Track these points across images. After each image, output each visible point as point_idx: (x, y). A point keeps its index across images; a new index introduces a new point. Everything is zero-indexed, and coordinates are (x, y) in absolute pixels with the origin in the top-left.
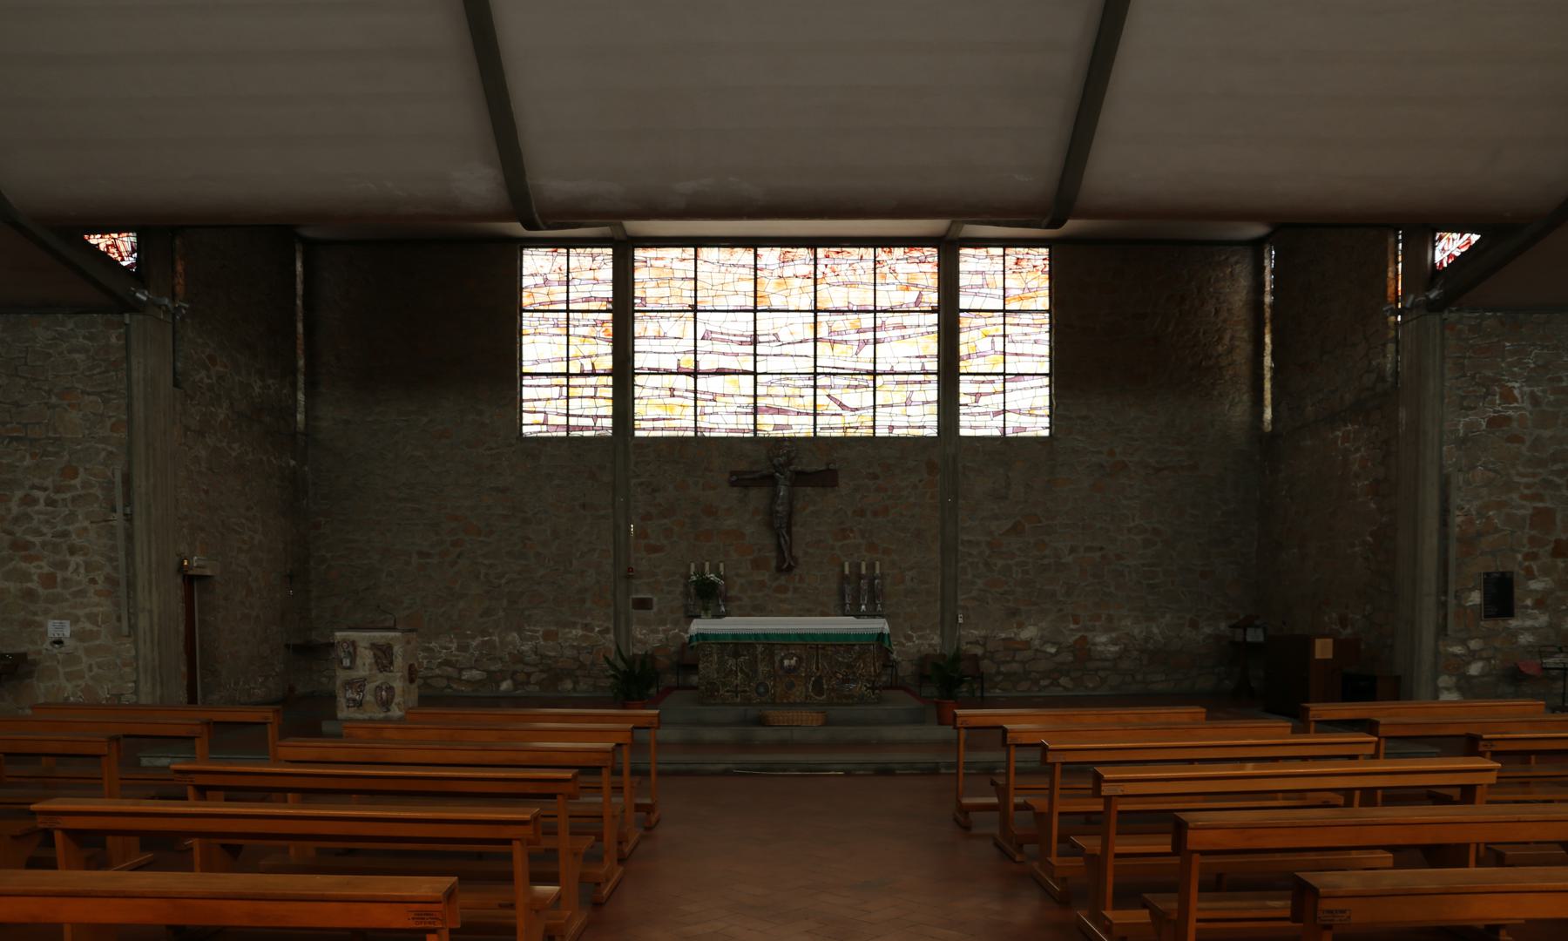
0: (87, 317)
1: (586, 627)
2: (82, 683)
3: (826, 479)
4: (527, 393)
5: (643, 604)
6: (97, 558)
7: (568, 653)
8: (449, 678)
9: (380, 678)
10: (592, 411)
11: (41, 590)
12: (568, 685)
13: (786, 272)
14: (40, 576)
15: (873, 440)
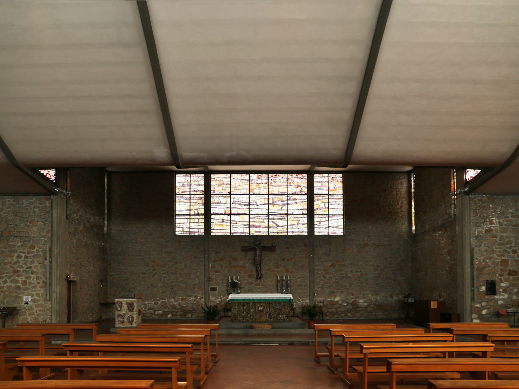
0: (39, 197)
1: (196, 297)
4: (177, 221)
5: (214, 289)
7: (189, 305)
8: (151, 314)
9: (129, 314)
10: (198, 227)
11: (22, 286)
12: (189, 316)
13: (259, 181)
14: (22, 281)
15: (287, 236)
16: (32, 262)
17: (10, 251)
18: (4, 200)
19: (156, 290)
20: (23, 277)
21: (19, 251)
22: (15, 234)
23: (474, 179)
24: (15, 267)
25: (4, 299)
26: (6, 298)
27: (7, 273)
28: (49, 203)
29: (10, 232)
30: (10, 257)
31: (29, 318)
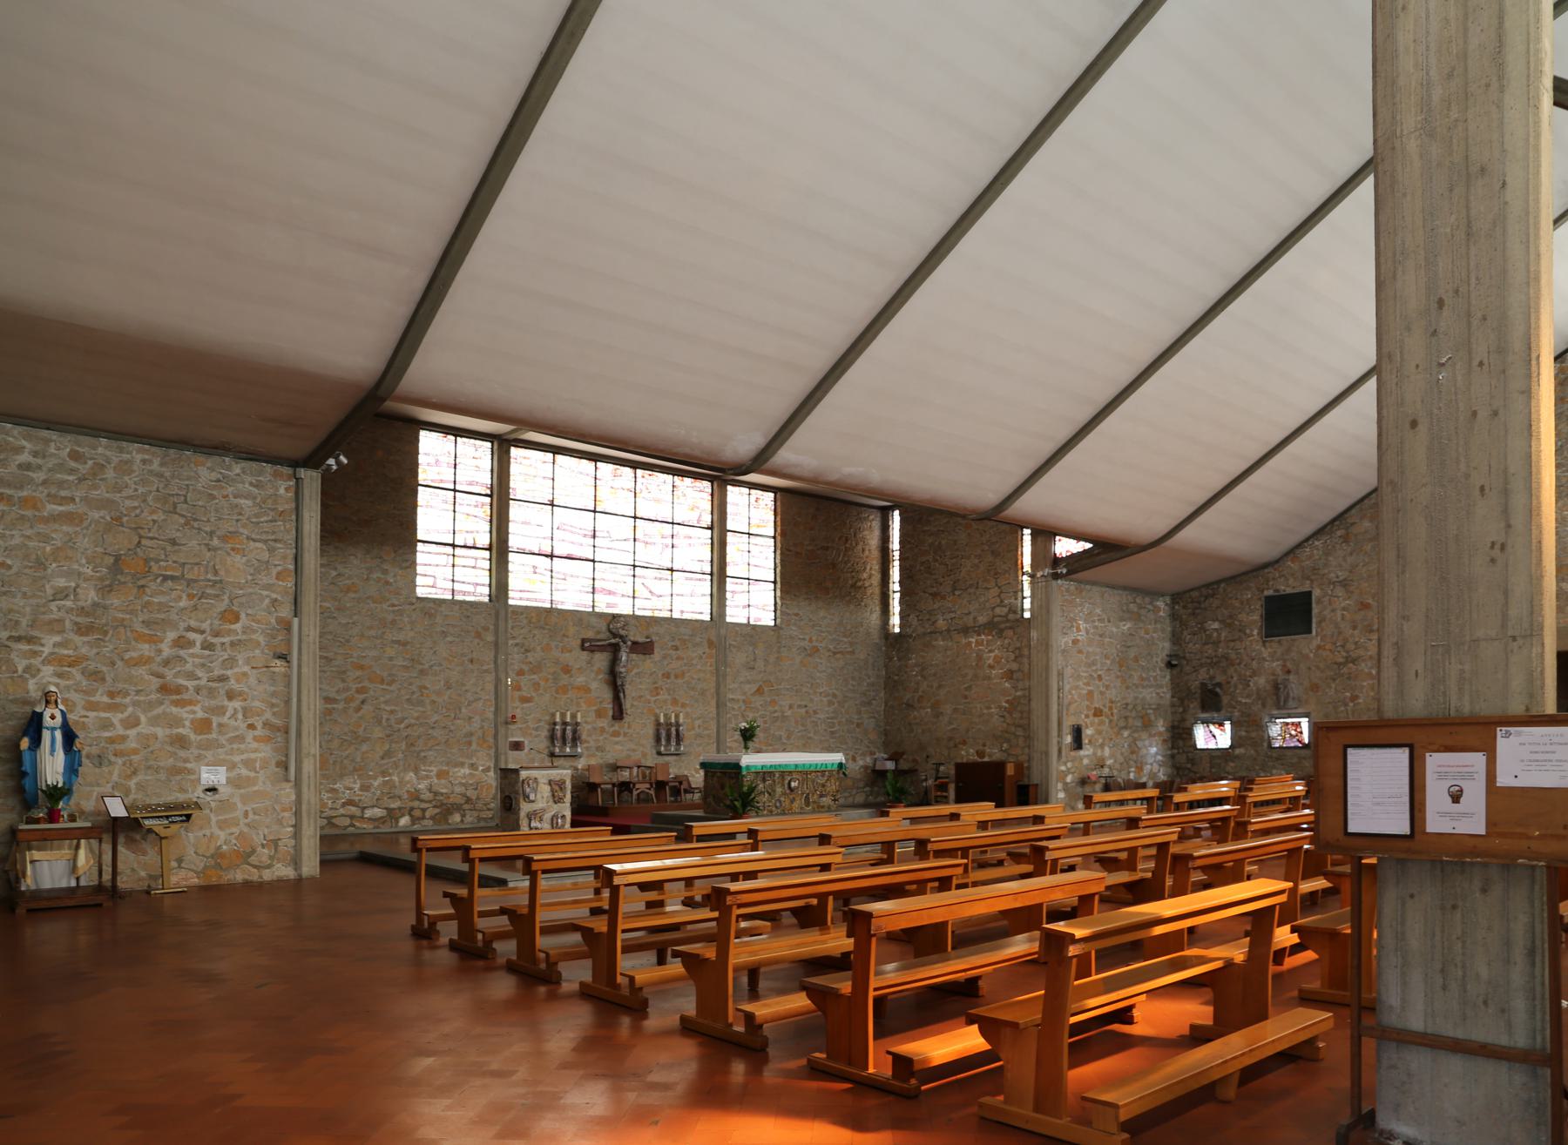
0: (254, 465)
1: (473, 766)
2: (236, 830)
3: (644, 648)
4: (420, 558)
6: (257, 704)
7: (458, 789)
8: (352, 817)
9: (555, 808)
10: (473, 582)
11: (193, 737)
12: (457, 818)
14: (192, 722)
15: (671, 619)
16: (230, 662)
17: (146, 623)
18: (126, 456)
19: (364, 747)
20: (197, 708)
21: (182, 625)
22: (165, 569)
23: (1073, 558)
24: (169, 674)
25: (129, 777)
26: (134, 773)
27: (138, 692)
28: (287, 489)
29: (146, 561)
30: (149, 642)
31: (222, 835)
